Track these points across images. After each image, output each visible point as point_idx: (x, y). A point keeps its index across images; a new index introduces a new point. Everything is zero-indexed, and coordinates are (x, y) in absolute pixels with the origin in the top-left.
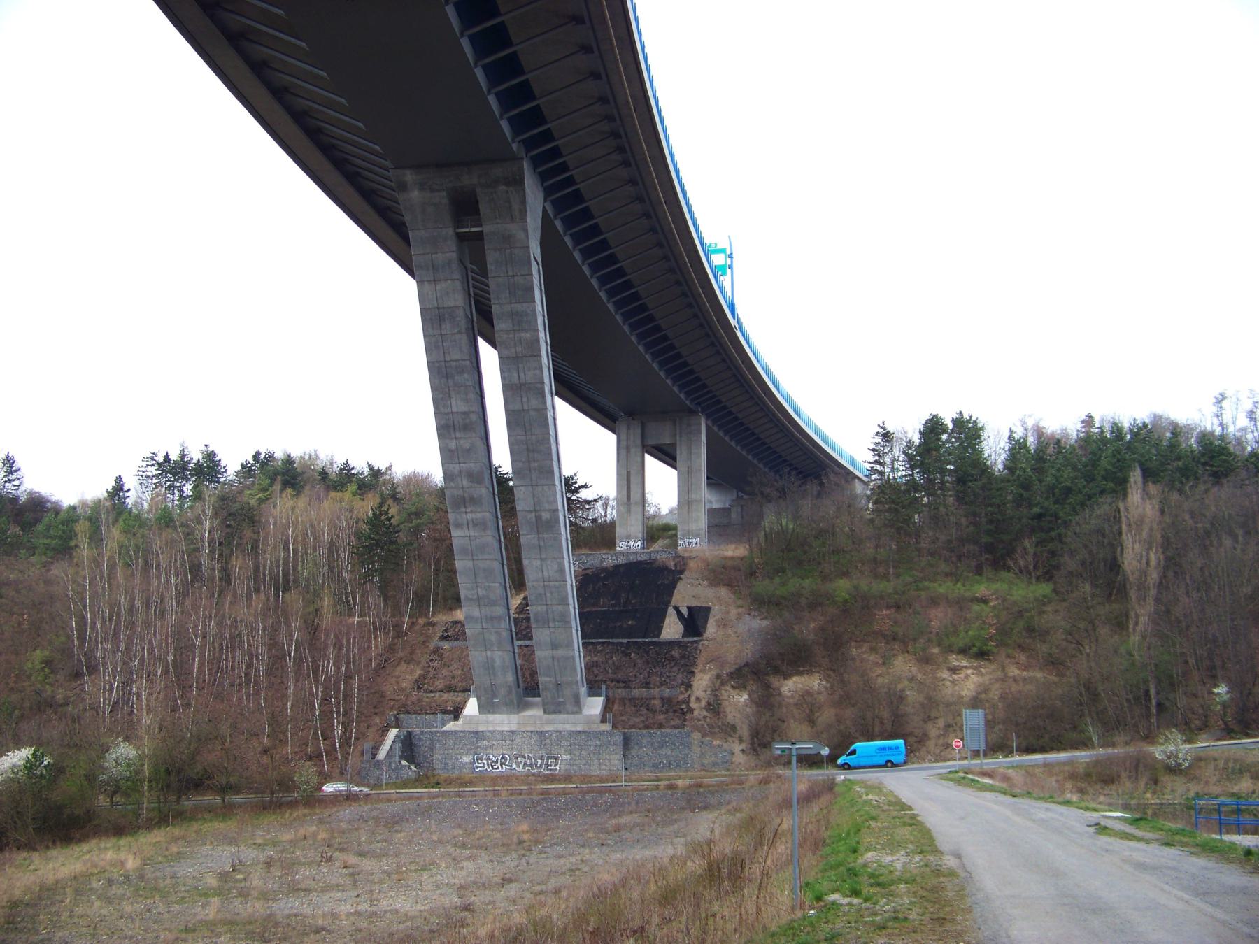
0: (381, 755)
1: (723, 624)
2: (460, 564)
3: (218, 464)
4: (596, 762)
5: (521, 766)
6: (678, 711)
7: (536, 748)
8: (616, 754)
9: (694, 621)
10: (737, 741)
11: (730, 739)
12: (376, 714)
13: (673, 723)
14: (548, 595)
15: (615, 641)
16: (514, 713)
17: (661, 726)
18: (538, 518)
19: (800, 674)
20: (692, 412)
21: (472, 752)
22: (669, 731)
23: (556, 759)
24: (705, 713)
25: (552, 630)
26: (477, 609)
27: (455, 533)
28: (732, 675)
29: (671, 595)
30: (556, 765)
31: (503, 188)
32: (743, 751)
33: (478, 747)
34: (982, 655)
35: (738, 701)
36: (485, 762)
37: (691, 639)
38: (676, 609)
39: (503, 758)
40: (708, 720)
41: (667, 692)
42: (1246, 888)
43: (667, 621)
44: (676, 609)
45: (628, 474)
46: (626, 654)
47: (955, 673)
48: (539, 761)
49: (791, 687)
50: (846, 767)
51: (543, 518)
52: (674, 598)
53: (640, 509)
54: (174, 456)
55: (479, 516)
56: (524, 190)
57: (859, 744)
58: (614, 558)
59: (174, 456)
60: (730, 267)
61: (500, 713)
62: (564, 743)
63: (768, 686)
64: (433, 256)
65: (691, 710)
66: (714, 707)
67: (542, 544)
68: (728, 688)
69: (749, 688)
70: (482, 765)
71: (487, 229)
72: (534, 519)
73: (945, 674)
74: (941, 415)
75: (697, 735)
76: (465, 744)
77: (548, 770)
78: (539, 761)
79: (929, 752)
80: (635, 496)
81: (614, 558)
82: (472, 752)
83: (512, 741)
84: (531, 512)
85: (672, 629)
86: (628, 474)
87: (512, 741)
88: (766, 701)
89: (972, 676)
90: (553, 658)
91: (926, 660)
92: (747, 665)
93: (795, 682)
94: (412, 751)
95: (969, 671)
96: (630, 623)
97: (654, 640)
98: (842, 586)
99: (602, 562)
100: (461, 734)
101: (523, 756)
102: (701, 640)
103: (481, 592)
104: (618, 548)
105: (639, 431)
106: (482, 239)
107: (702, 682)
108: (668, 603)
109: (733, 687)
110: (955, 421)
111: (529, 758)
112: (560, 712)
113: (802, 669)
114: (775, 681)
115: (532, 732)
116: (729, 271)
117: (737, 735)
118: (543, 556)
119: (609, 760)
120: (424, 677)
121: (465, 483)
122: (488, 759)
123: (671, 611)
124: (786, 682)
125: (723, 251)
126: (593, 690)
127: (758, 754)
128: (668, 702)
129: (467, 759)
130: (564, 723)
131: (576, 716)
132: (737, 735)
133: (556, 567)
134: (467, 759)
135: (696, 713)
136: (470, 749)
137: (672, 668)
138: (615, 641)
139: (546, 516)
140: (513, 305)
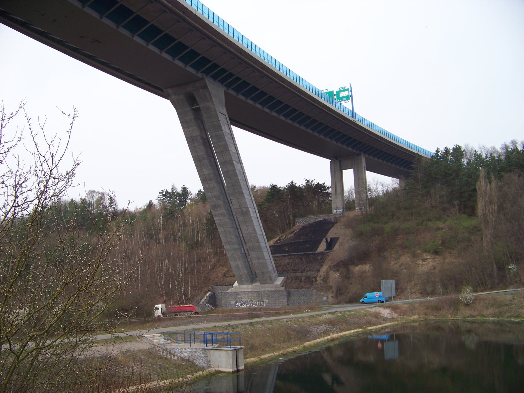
0: (201, 303)
1: (341, 245)
2: (220, 230)
3: (187, 192)
4: (278, 302)
5: (252, 305)
6: (310, 281)
7: (256, 297)
8: (285, 299)
9: (330, 245)
10: (331, 293)
11: (328, 292)
12: (206, 286)
13: (307, 286)
14: (252, 239)
15: (299, 253)
16: (250, 285)
17: (302, 288)
18: (242, 211)
19: (362, 264)
20: (359, 155)
21: (235, 300)
22: (304, 289)
23: (263, 302)
24: (321, 282)
25: (256, 252)
26: (229, 246)
27: (215, 218)
28: (334, 266)
29: (327, 233)
30: (263, 304)
31: (201, 90)
32: (332, 297)
33: (237, 298)
34: (436, 252)
35: (335, 275)
36: (239, 303)
37: (328, 251)
38: (326, 239)
39: (245, 302)
40: (322, 284)
41: (309, 273)
42: (244, 355)
43: (322, 244)
44: (326, 239)
45: (335, 182)
46: (301, 259)
47: (424, 261)
48: (258, 303)
49: (357, 269)
50: (363, 303)
51: (244, 211)
52: (328, 234)
53: (340, 196)
54: (170, 191)
55: (222, 211)
56: (208, 90)
57: (367, 294)
58: (320, 218)
59: (170, 191)
60: (351, 96)
61: (245, 285)
62: (266, 295)
63: (348, 270)
64: (186, 118)
65: (316, 281)
66: (325, 279)
67: (246, 220)
68: (332, 271)
69: (340, 271)
70: (238, 305)
71: (201, 106)
72: (240, 211)
73: (420, 262)
74: (448, 147)
75: (315, 291)
76: (232, 297)
77: (261, 306)
78: (258, 303)
79: (404, 296)
80: (339, 190)
81: (320, 218)
82: (235, 300)
83: (248, 295)
84: (239, 208)
85: (322, 247)
86: (335, 182)
87: (248, 295)
88: (347, 276)
89: (431, 262)
90: (259, 263)
91: (415, 256)
92: (341, 261)
93: (359, 268)
94: (215, 300)
95: (430, 260)
96: (307, 246)
97: (313, 252)
98: (388, 228)
99: (315, 220)
100: (231, 293)
101: (252, 301)
102: (330, 252)
103: (229, 240)
104: (333, 213)
105: (338, 165)
106: (200, 110)
107: (325, 268)
108: (324, 236)
109: (334, 271)
110: (454, 149)
111: (254, 302)
112: (266, 283)
113: (363, 262)
114: (351, 268)
115: (255, 291)
116: (350, 98)
117: (332, 290)
118: (247, 225)
119: (282, 302)
120: (227, 271)
121: (215, 200)
122: (240, 302)
123: (324, 240)
124: (356, 268)
125: (347, 90)
126: (280, 274)
127: (337, 298)
128: (308, 278)
129: (233, 303)
130: (268, 288)
131: (272, 285)
132: (332, 290)
133: (252, 229)
134: (233, 303)
135: (318, 282)
136: (234, 299)
137: (315, 264)
138: (299, 253)
139: (244, 210)
140: (216, 133)
